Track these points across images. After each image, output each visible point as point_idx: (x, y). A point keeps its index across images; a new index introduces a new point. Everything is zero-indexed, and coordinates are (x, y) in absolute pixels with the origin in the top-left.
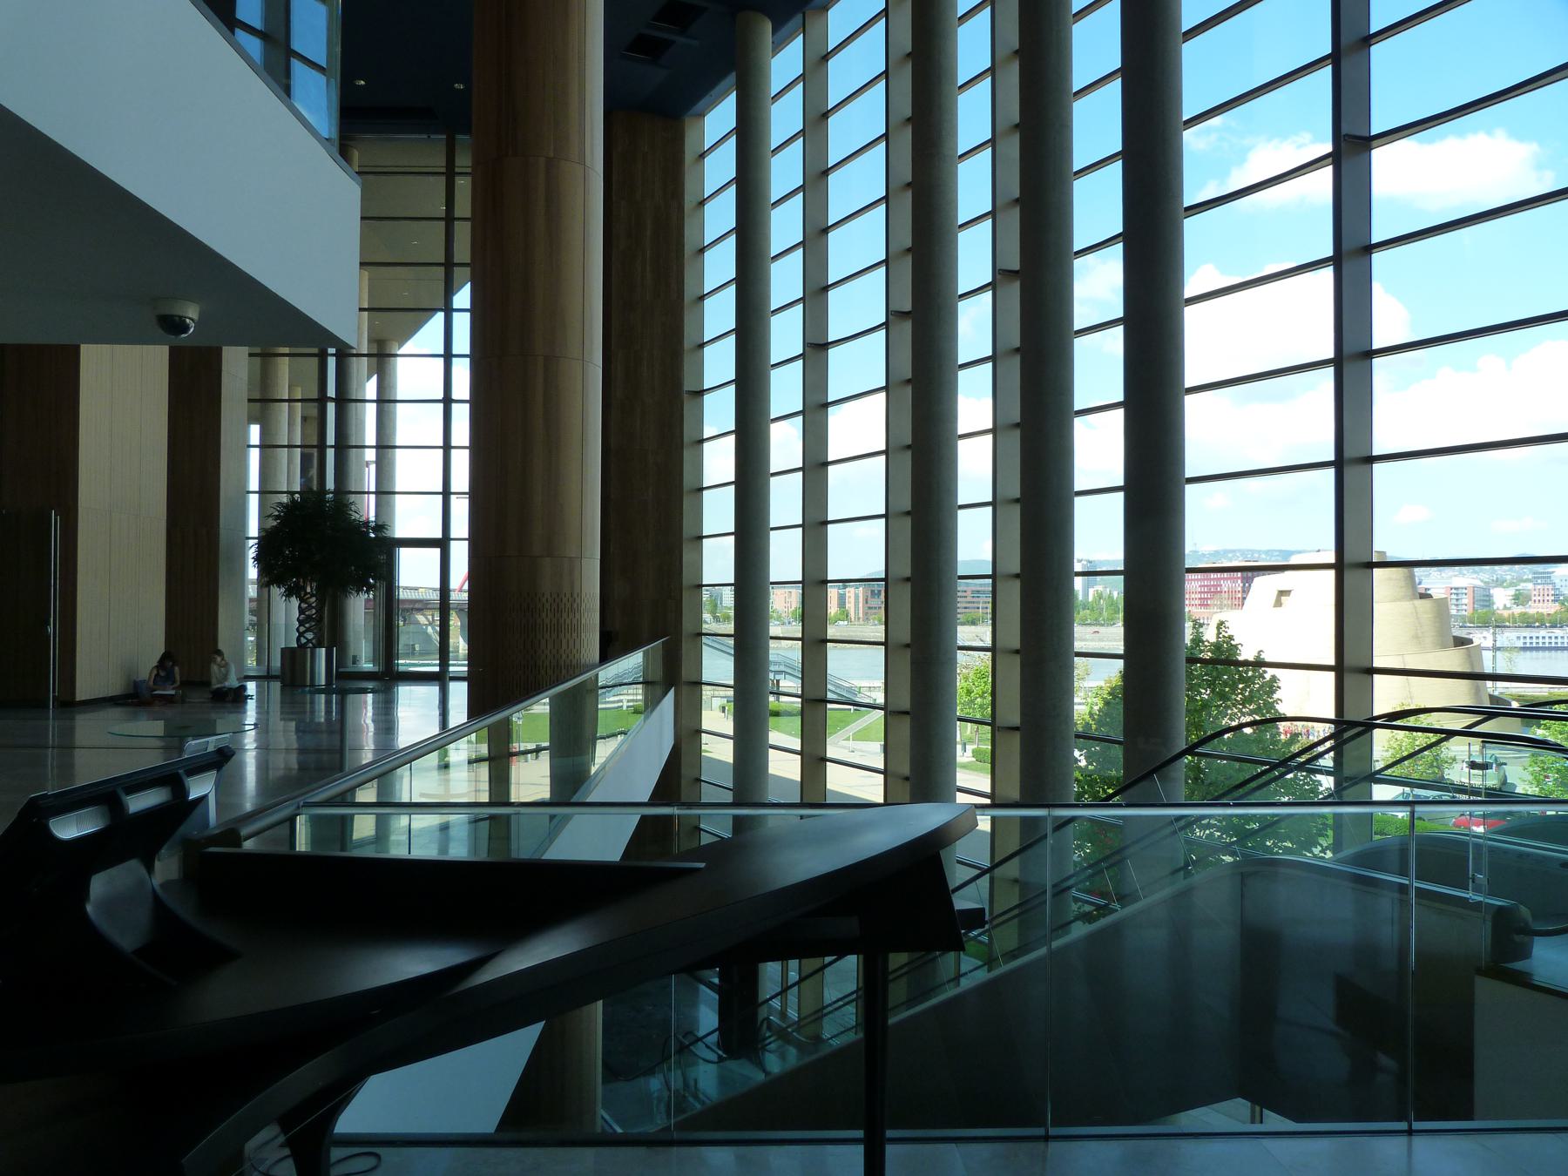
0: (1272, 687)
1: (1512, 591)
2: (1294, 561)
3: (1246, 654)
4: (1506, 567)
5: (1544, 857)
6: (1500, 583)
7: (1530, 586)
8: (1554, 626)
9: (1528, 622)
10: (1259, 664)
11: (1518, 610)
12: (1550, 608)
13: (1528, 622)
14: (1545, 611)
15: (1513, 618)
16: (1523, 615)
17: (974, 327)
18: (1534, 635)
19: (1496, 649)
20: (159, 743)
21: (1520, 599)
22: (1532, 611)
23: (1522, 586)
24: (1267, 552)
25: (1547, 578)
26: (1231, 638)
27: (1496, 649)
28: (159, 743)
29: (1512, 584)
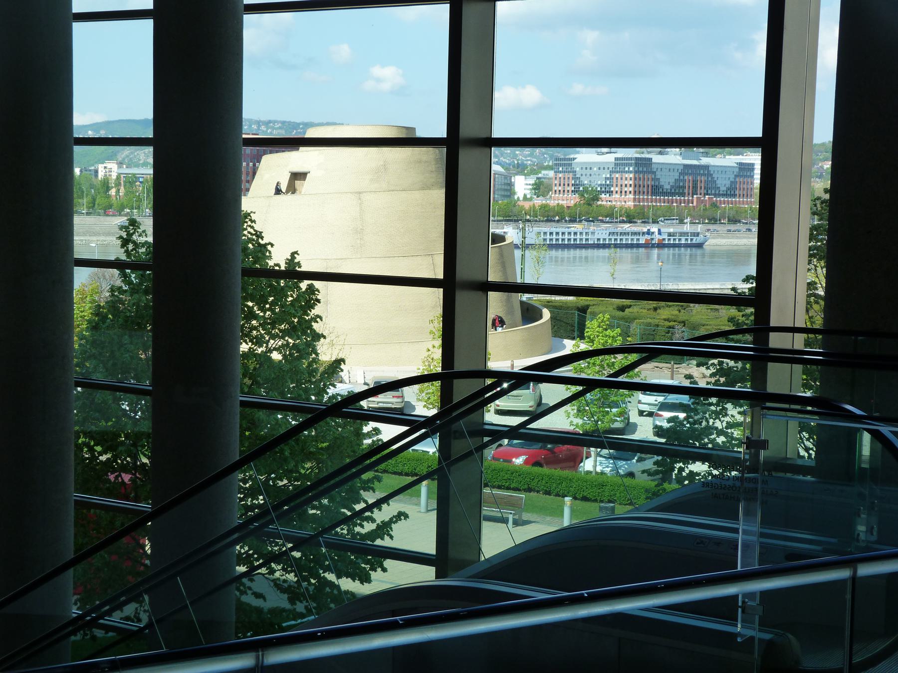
0: (310, 300)
1: (532, 180)
2: (311, 134)
3: (278, 258)
4: (527, 151)
5: (710, 539)
6: (521, 169)
7: (551, 174)
8: (573, 221)
9: (549, 215)
10: (293, 273)
11: (538, 202)
12: (570, 200)
13: (549, 215)
14: (564, 203)
15: (533, 212)
16: (544, 207)
17: (55, 637)
18: (554, 230)
19: (525, 246)
20: (531, 187)
21: (540, 188)
22: (552, 203)
23: (544, 173)
24: (268, 123)
25: (567, 164)
26: (259, 235)
27: (525, 246)
28: (531, 187)
29: (533, 172)
